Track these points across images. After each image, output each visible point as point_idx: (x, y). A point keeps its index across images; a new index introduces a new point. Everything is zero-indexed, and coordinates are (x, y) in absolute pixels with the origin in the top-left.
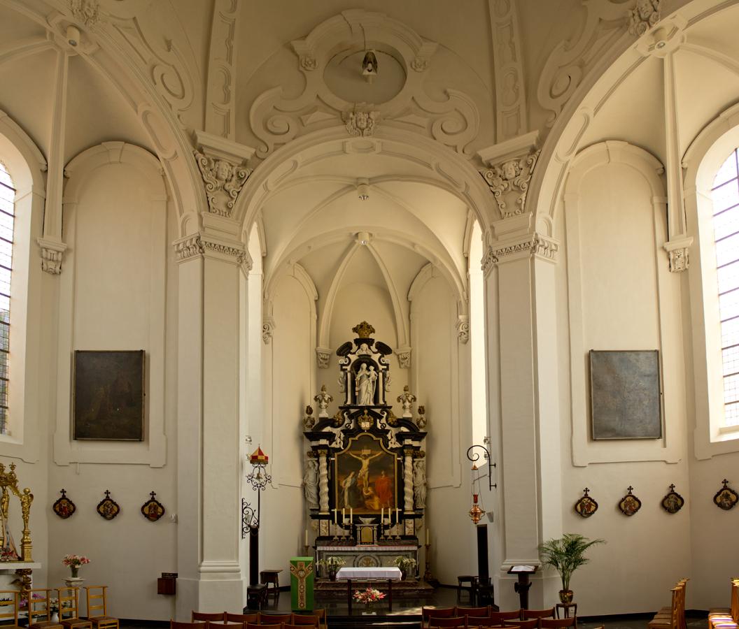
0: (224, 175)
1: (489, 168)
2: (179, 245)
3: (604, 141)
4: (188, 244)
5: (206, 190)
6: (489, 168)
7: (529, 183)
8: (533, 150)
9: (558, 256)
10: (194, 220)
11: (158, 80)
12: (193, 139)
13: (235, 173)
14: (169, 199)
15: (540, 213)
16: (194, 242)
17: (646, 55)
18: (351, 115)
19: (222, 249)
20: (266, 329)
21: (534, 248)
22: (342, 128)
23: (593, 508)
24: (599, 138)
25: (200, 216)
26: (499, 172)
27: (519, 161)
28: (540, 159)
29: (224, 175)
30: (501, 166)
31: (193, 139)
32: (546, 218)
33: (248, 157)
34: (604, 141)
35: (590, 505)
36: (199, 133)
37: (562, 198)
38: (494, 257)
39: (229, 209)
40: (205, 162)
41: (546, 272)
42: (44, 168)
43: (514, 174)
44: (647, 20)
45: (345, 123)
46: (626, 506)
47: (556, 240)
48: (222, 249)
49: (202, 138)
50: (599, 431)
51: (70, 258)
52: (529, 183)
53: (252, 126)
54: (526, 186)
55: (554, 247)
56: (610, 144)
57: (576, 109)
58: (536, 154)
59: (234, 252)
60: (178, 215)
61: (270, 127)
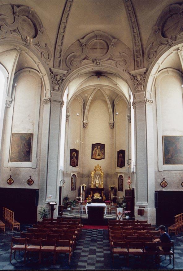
0: (58, 79)
1: (134, 77)
2: (44, 100)
3: (166, 68)
4: (47, 100)
5: (53, 84)
6: (134, 77)
7: (144, 83)
8: (145, 73)
9: (154, 103)
10: (49, 92)
11: (42, 55)
12: (50, 70)
13: (61, 78)
14: (42, 85)
15: (148, 91)
16: (49, 100)
17: (172, 52)
18: (95, 61)
19: (56, 101)
20: (67, 117)
21: (146, 102)
22: (93, 64)
23: (32, 182)
24: (165, 67)
25: (51, 92)
26: (136, 78)
27: (141, 76)
28: (147, 76)
29: (58, 79)
30: (136, 77)
31: (50, 70)
32: (150, 93)
33: (65, 74)
34: (166, 68)
35: (31, 181)
36: (52, 69)
37: (155, 85)
38: (135, 104)
39: (59, 90)
40: (53, 76)
41: (149, 108)
42: (8, 76)
43: (140, 79)
44: (171, 45)
45: (93, 63)
46: (163, 184)
47: (153, 99)
48: (56, 101)
49: (53, 70)
50: (168, 160)
51: (13, 102)
52: (144, 83)
53: (67, 64)
54: (143, 83)
55: (152, 102)
56: (168, 69)
57: (155, 63)
58: (146, 73)
59: (59, 102)
60: (45, 90)
61: (72, 63)
